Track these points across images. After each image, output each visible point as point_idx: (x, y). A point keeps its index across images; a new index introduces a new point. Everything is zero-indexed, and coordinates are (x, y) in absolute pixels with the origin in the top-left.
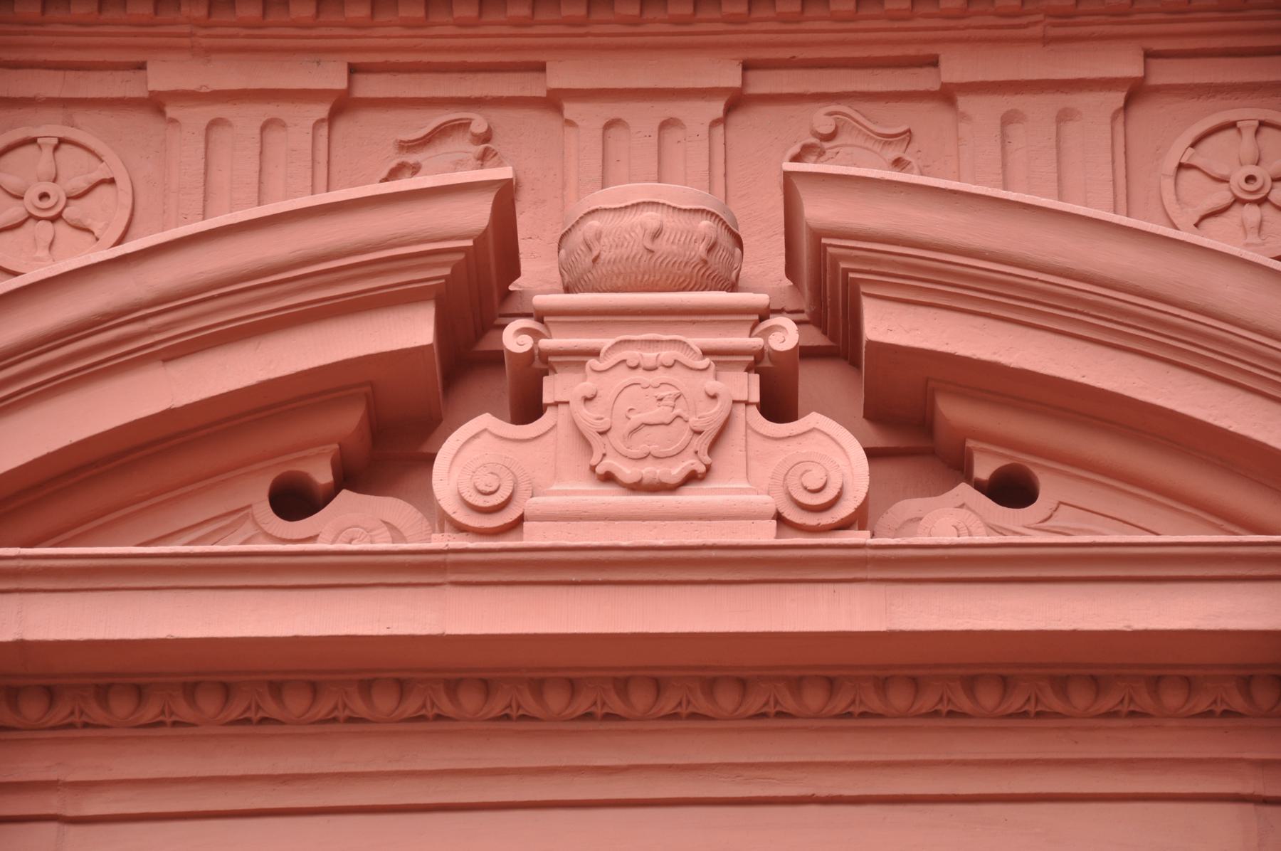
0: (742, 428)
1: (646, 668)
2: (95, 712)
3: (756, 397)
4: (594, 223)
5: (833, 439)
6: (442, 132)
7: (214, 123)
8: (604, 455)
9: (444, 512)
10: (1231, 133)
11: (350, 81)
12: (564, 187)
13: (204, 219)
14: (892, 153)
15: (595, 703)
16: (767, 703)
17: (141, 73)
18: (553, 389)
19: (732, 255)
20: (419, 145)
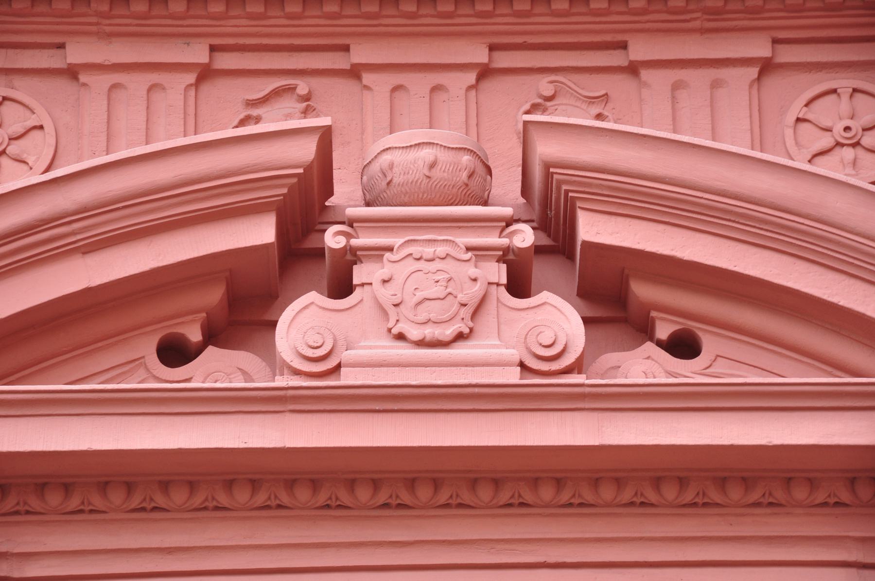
0: (495, 302)
1: (427, 471)
2: (35, 503)
3: (504, 281)
4: (387, 157)
5: (559, 310)
6: (276, 93)
7: (114, 87)
8: (398, 321)
9: (284, 361)
10: (833, 97)
11: (211, 57)
12: (363, 132)
13: (107, 154)
14: (595, 110)
15: (391, 497)
16: (512, 497)
17: (60, 52)
18: (359, 274)
19: (485, 180)
20: (260, 103)
